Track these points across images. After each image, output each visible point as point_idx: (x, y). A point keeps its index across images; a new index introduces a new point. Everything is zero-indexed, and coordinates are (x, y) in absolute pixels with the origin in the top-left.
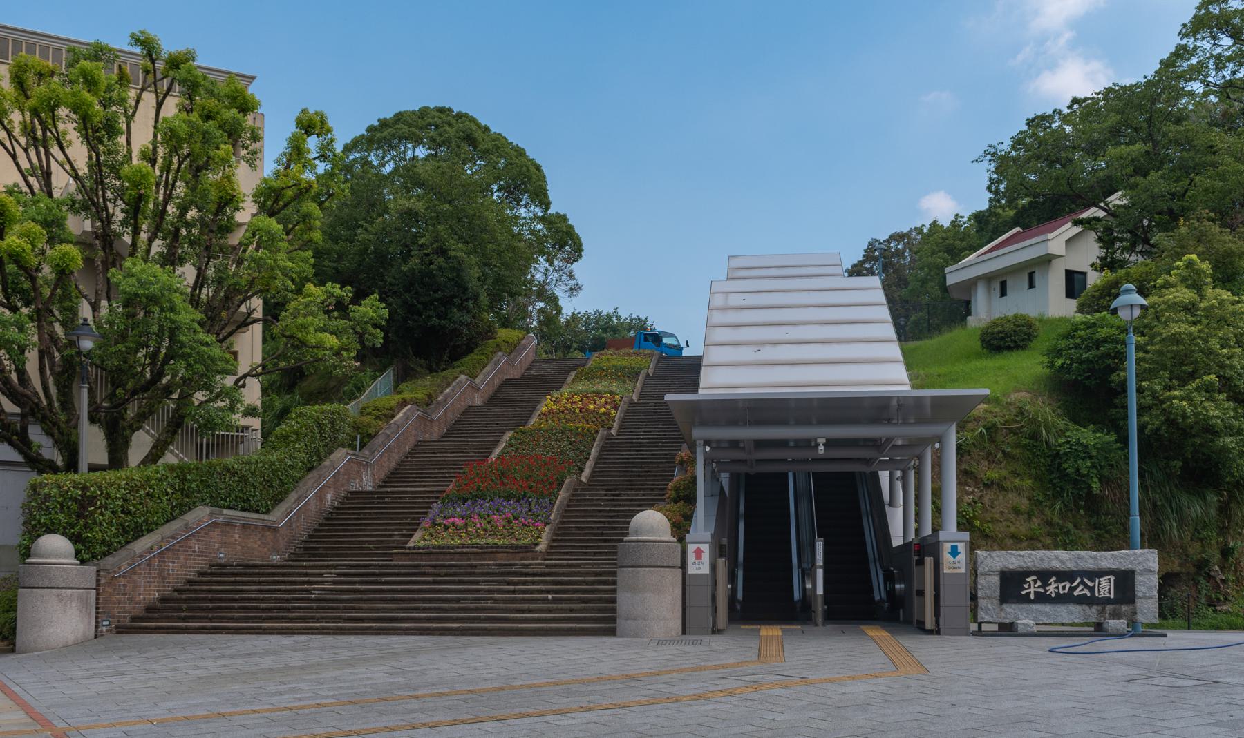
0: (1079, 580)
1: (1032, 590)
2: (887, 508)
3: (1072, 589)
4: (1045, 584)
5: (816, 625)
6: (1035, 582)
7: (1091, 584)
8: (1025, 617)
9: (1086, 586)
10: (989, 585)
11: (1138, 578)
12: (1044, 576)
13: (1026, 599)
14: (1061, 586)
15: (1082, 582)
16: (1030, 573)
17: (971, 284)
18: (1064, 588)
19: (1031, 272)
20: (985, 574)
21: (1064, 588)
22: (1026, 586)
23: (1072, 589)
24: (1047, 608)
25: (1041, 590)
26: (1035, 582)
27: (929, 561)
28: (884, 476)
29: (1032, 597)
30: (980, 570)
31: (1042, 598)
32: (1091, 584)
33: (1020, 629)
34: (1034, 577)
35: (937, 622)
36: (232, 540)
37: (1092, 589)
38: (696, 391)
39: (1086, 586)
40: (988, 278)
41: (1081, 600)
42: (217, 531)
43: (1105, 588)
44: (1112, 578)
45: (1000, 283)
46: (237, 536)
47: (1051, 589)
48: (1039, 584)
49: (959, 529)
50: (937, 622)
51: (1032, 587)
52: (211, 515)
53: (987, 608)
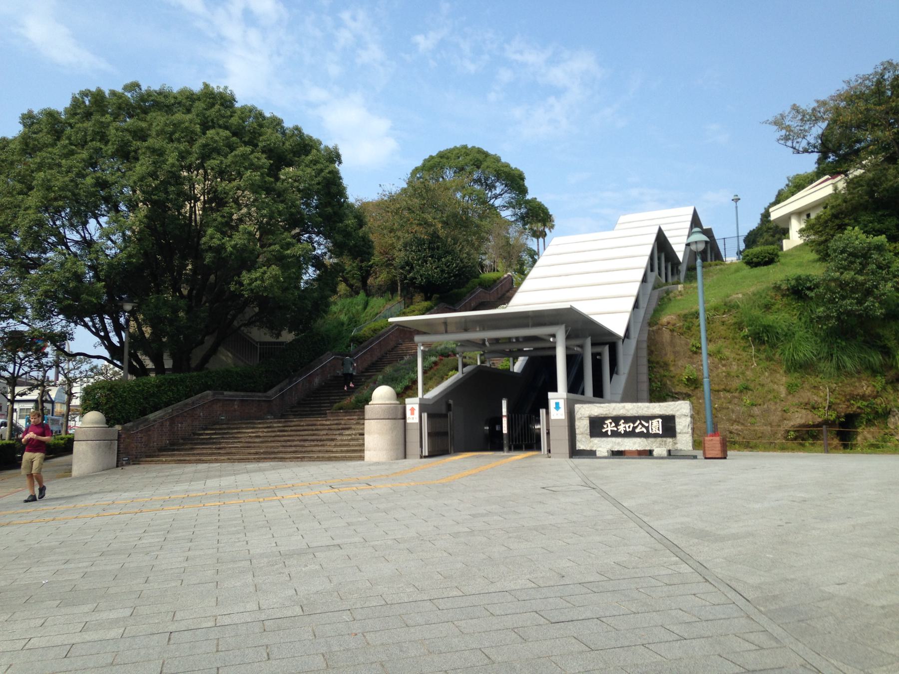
3: (634, 428)
4: (617, 425)
7: (646, 425)
8: (603, 446)
11: (677, 420)
12: (616, 420)
13: (605, 435)
14: (627, 426)
16: (607, 418)
24: (619, 440)
31: (615, 434)
32: (646, 425)
33: (598, 454)
37: (647, 428)
41: (641, 435)
43: (656, 426)
44: (660, 420)
47: (621, 428)
48: (613, 424)
51: (609, 427)
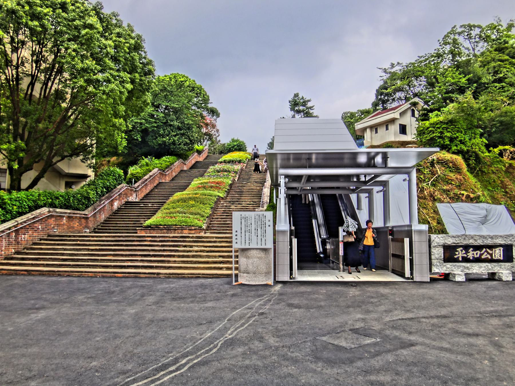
0: (484, 250)
1: (460, 255)
2: (357, 211)
3: (481, 255)
4: (467, 252)
5: (338, 269)
6: (462, 251)
8: (458, 271)
9: (488, 253)
10: (438, 253)
13: (456, 261)
14: (475, 253)
15: (486, 251)
17: (364, 130)
18: (477, 254)
19: (387, 124)
20: (435, 247)
21: (477, 254)
22: (457, 253)
23: (481, 255)
24: (468, 265)
25: (465, 255)
26: (462, 251)
27: (407, 241)
28: (353, 197)
29: (460, 259)
30: (433, 244)
31: (466, 260)
32: (490, 252)
34: (461, 249)
35: (412, 274)
36: (62, 223)
37: (491, 255)
38: (271, 249)
39: (488, 253)
40: (371, 127)
42: (53, 219)
44: (502, 249)
45: (375, 128)
46: (65, 221)
48: (464, 252)
49: (419, 222)
50: (412, 274)
51: (460, 254)
52: (49, 212)
53: (437, 265)
